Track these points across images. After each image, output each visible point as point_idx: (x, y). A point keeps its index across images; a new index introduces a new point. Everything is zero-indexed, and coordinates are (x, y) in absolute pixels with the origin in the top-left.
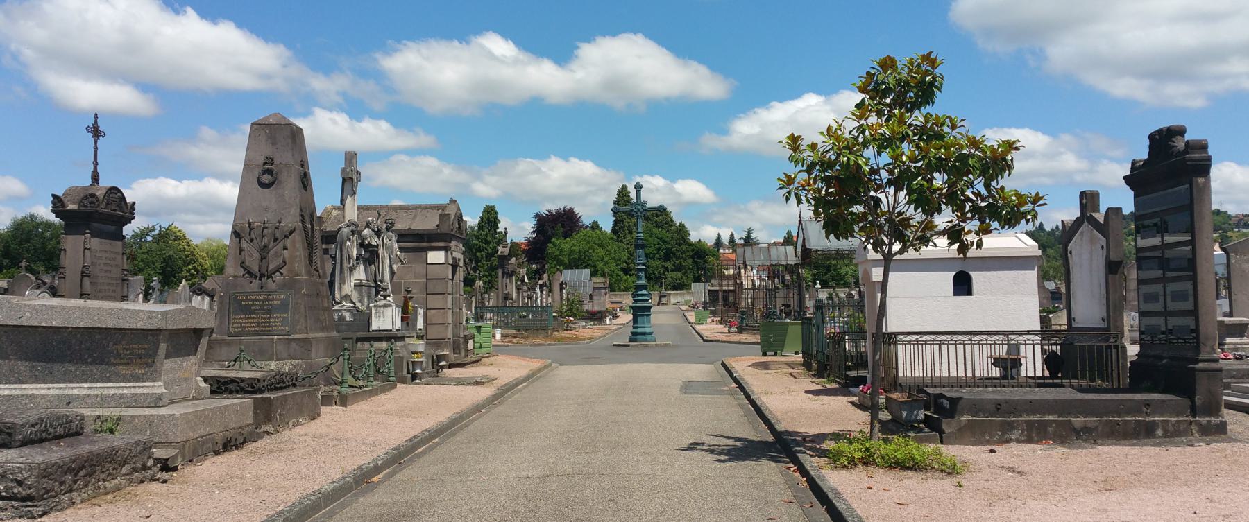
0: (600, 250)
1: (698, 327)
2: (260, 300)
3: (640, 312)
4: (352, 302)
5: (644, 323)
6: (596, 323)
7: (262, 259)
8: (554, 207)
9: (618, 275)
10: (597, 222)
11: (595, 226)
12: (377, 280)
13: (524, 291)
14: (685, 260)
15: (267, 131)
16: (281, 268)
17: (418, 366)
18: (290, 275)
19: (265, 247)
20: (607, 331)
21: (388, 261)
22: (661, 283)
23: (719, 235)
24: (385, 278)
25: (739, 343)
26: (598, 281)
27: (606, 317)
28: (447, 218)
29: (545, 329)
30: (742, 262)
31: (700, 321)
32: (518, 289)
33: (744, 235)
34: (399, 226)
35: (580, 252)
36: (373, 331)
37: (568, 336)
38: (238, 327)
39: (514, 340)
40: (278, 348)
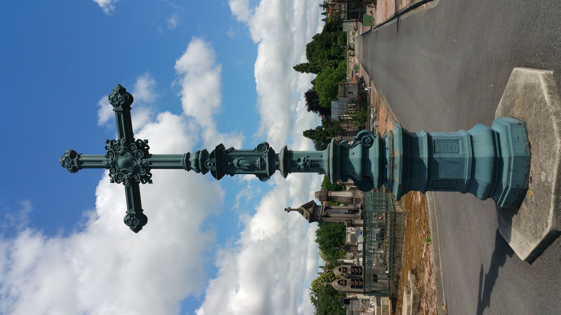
5: (460, 162)
10: (311, 81)
11: (313, 82)
22: (343, 48)
23: (322, 20)
26: (340, 88)
35: (326, 91)
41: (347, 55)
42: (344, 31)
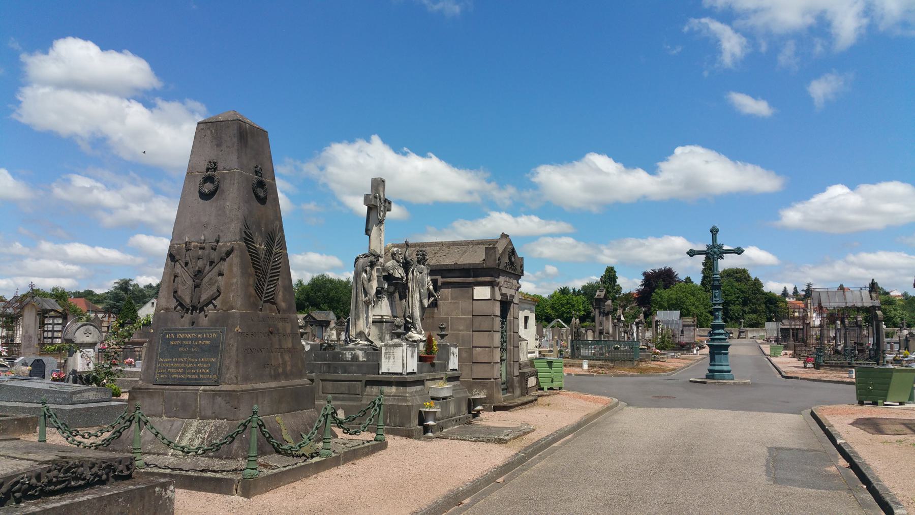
0: (692, 297)
1: (774, 360)
2: (189, 339)
3: (718, 351)
4: (368, 340)
5: (721, 362)
6: (685, 352)
7: (195, 287)
8: (657, 268)
9: (705, 316)
11: (688, 280)
12: (406, 316)
13: (621, 327)
14: (759, 305)
15: (213, 131)
16: (215, 299)
17: (431, 417)
18: (224, 309)
19: (199, 271)
20: (691, 362)
21: (418, 295)
22: (741, 322)
23: (785, 288)
24: (415, 314)
25: (820, 381)
27: (693, 348)
28: (492, 251)
29: (631, 360)
30: (817, 305)
31: (775, 354)
32: (615, 326)
33: (805, 288)
34: (433, 261)
35: (676, 299)
36: (383, 373)
37: (654, 366)
38: (163, 373)
39: (600, 371)
40: (202, 402)
41: (730, 329)
42: (766, 323)
